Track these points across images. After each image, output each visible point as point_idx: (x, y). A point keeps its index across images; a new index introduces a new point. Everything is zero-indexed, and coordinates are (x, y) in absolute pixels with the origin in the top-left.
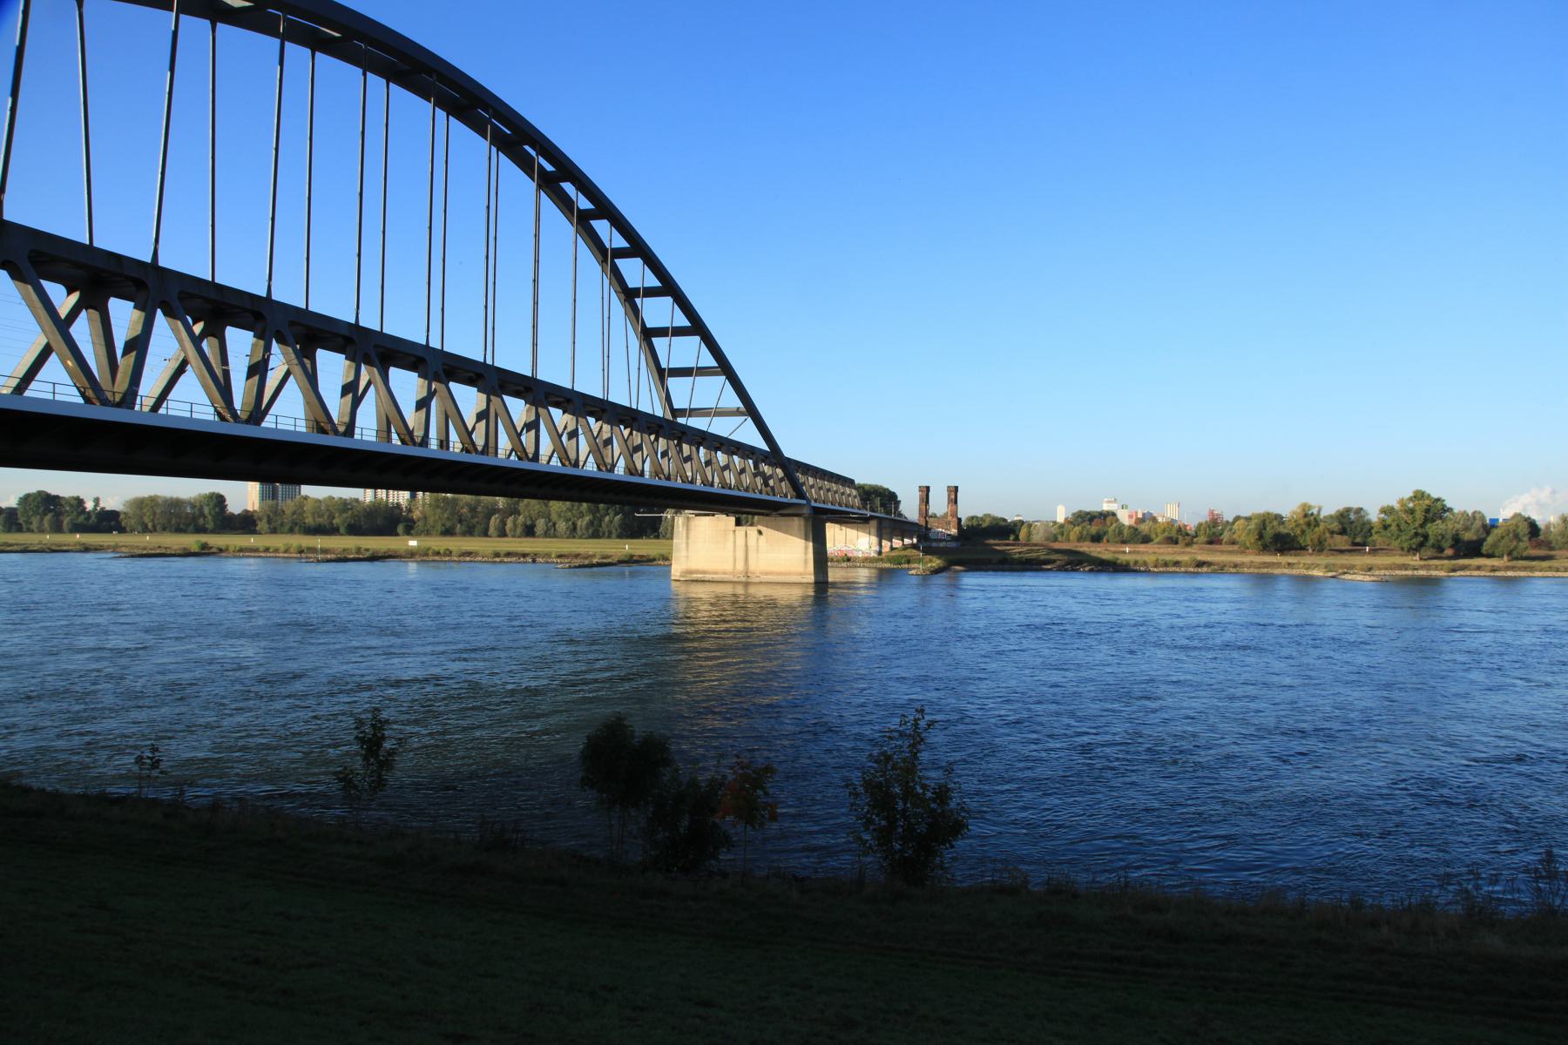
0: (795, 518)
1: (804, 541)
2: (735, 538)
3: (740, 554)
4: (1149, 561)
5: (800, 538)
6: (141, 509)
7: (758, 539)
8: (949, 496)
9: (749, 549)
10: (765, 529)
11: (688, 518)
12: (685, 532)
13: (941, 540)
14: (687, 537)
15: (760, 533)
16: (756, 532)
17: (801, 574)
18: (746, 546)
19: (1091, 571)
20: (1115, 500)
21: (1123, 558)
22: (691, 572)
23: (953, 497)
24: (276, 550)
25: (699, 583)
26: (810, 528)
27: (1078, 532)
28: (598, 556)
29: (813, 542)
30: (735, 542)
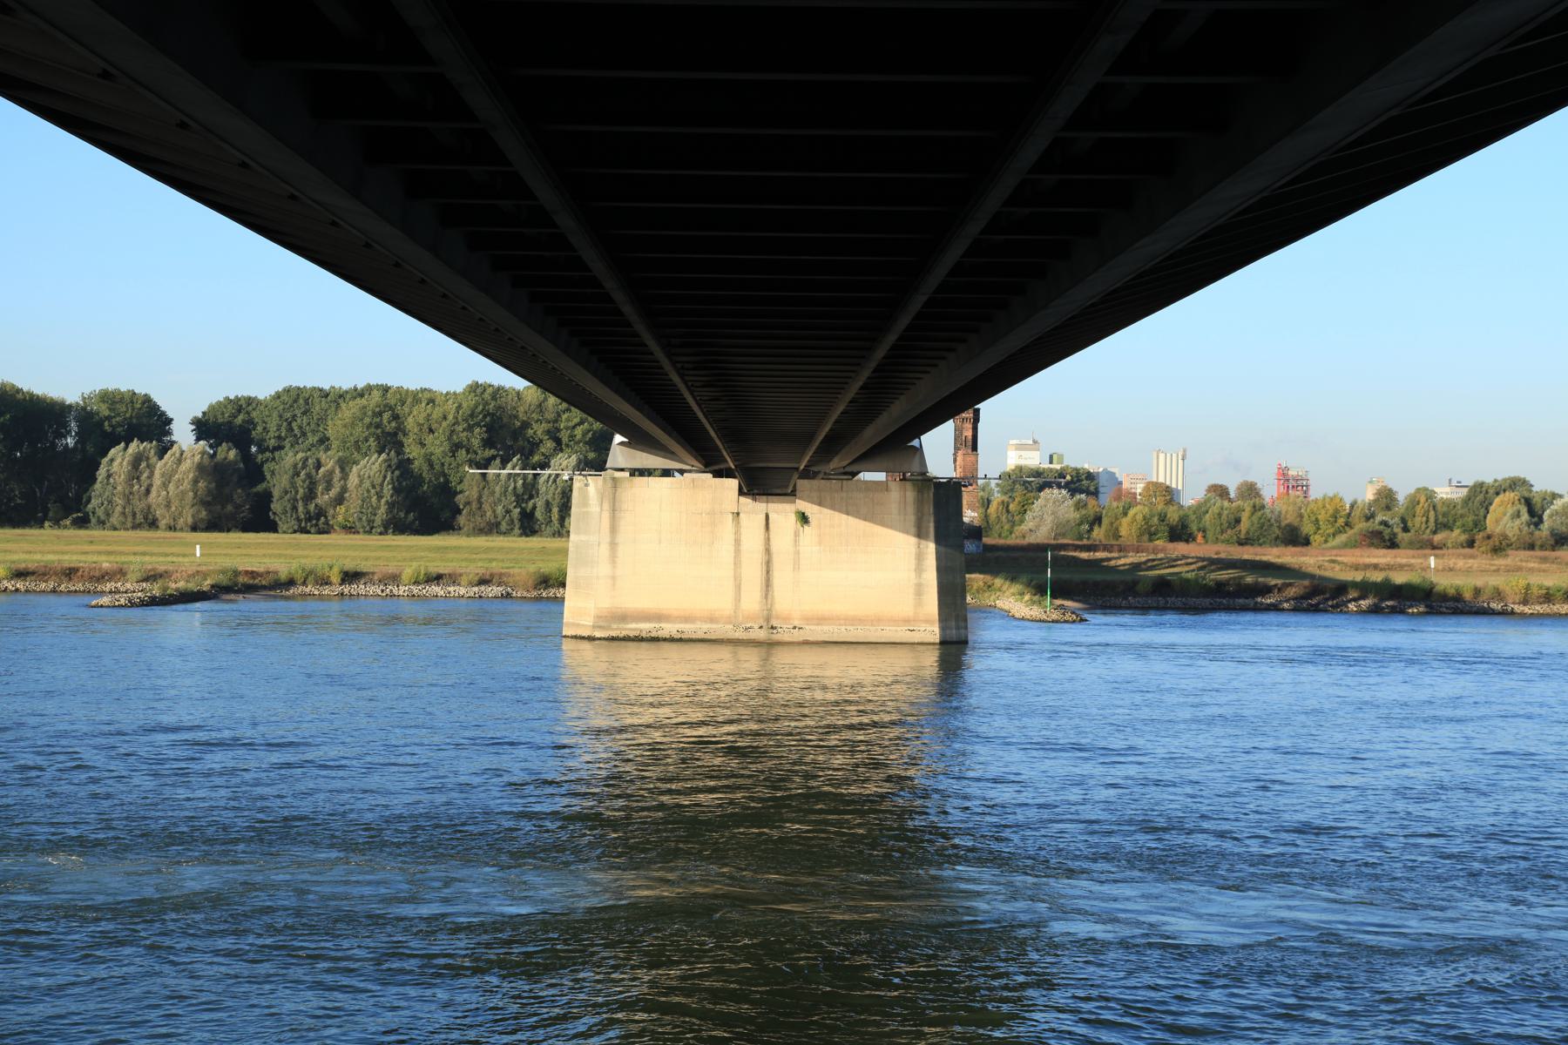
1: (913, 540)
2: (737, 533)
4: (1508, 590)
5: (906, 532)
6: (1087, 478)
7: (796, 534)
10: (816, 508)
11: (614, 479)
12: (606, 516)
14: (614, 529)
15: (804, 519)
16: (793, 518)
17: (907, 621)
18: (768, 551)
19: (1375, 610)
20: (1035, 442)
21: (1444, 583)
22: (624, 617)
23: (969, 433)
24: (395, 579)
25: (630, 644)
26: (929, 509)
27: (1139, 517)
28: (132, 577)
29: (938, 541)
30: (737, 542)
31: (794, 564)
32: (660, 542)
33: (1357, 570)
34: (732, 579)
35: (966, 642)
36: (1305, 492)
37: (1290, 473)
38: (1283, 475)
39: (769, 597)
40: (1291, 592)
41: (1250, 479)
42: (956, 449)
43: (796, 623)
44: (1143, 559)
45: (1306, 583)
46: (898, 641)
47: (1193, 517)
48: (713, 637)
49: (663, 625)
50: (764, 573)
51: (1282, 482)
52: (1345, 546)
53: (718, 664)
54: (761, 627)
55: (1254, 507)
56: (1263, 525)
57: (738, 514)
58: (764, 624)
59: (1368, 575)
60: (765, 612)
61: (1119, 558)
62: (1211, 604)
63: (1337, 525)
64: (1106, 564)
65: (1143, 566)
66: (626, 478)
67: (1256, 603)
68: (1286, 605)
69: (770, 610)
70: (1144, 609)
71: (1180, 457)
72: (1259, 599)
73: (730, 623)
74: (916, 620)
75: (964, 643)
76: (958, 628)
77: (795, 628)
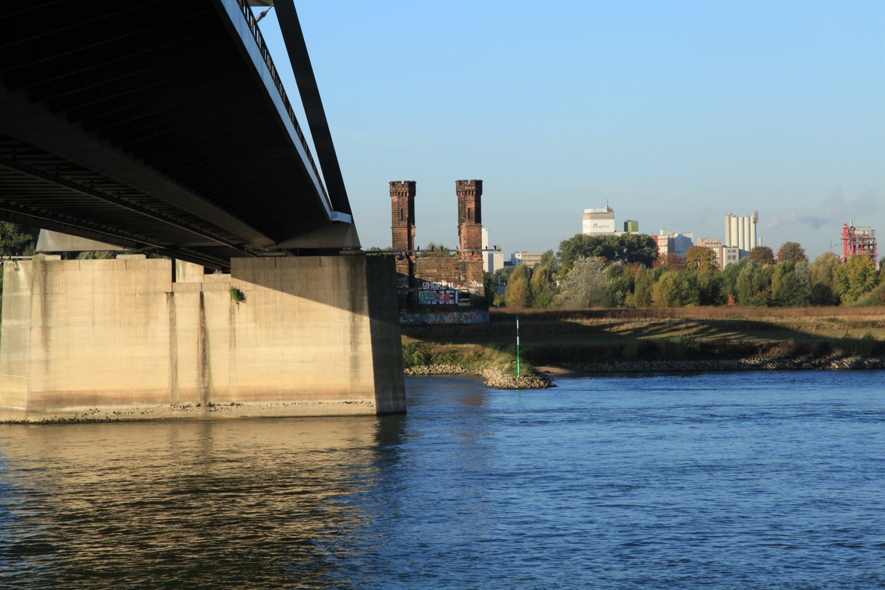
0: (325, 259)
1: (347, 314)
3: (189, 351)
5: (340, 306)
6: (648, 245)
7: (232, 312)
8: (462, 204)
9: (212, 337)
11: (45, 264)
12: (37, 299)
13: (446, 309)
14: (45, 313)
15: (239, 296)
16: (227, 295)
17: (343, 394)
18: (203, 329)
19: (857, 367)
20: (609, 210)
22: (59, 400)
23: (472, 206)
26: (363, 283)
27: (670, 282)
29: (372, 315)
30: (173, 321)
31: (230, 341)
32: (93, 325)
33: (855, 327)
34: (168, 359)
35: (404, 412)
36: (872, 251)
37: (856, 232)
38: (850, 235)
39: (207, 375)
40: (775, 352)
41: (793, 240)
42: (461, 221)
43: (234, 400)
44: (646, 324)
45: (791, 342)
46: (335, 414)
47: (727, 280)
48: (150, 418)
49: (99, 407)
50: (201, 351)
51: (848, 242)
52: (869, 303)
53: (159, 439)
54: (199, 405)
55: (784, 268)
56: (792, 286)
57: (172, 293)
58: (202, 402)
59: (850, 332)
60: (202, 390)
61: (622, 324)
62: (695, 366)
63: (867, 283)
64: (608, 329)
65: (645, 331)
66: (58, 261)
67: (740, 363)
68: (769, 366)
69: (207, 388)
70: (632, 374)
71: (752, 220)
72: (743, 361)
73: (167, 402)
74: (354, 393)
75: (402, 413)
76: (396, 399)
77: (232, 404)
